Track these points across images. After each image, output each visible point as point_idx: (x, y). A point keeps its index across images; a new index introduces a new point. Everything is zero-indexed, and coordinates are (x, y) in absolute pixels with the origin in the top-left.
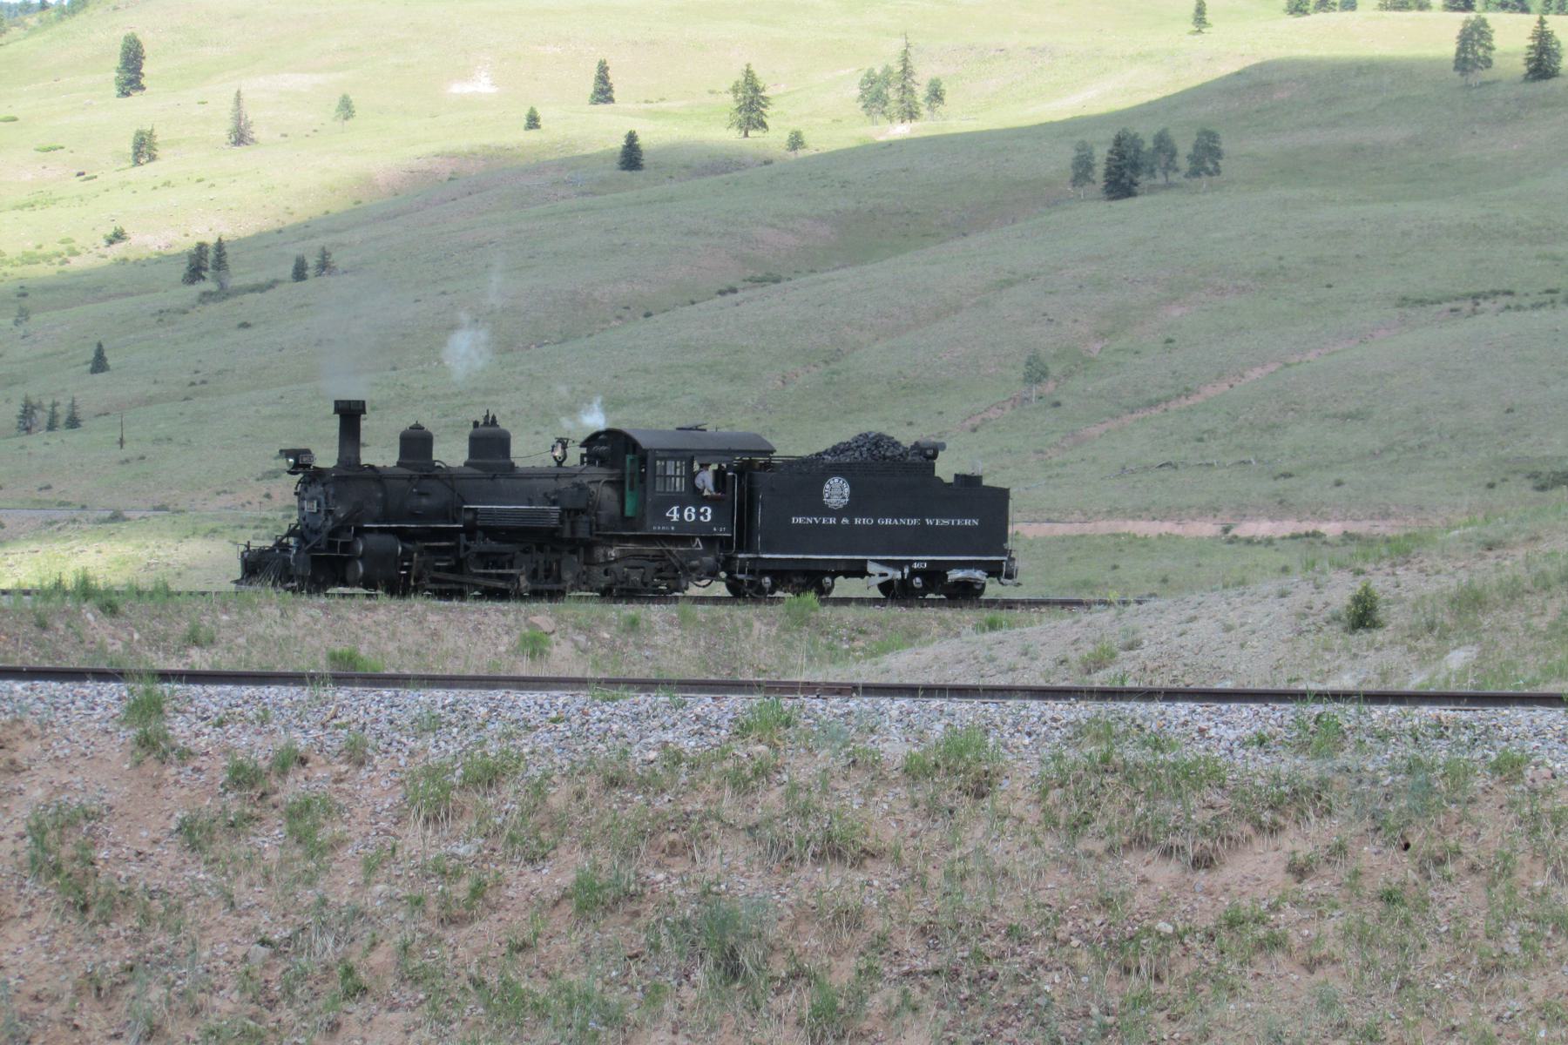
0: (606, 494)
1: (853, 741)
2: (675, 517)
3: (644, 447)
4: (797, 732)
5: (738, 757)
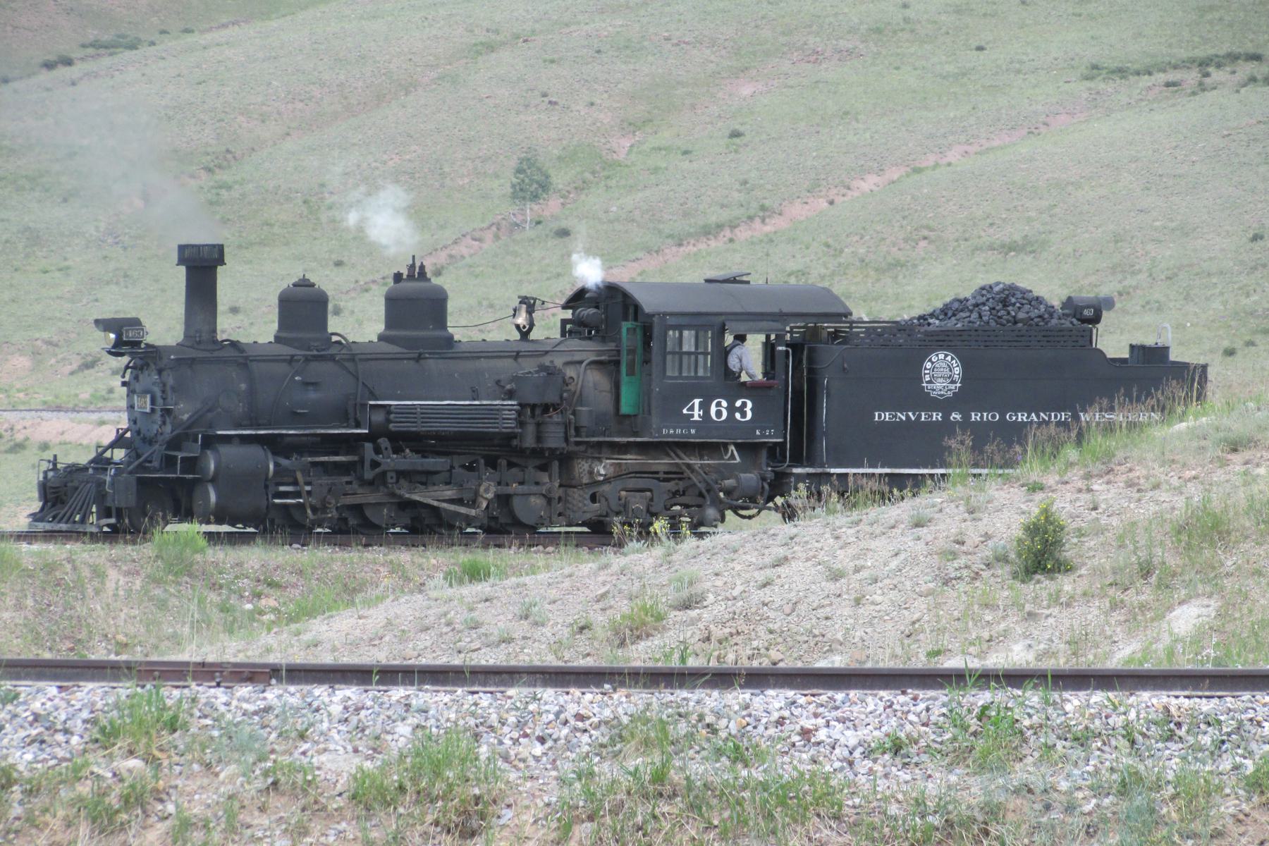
0: (594, 382)
1: (273, 751)
2: (697, 415)
3: (647, 309)
4: (188, 739)
5: (99, 777)
